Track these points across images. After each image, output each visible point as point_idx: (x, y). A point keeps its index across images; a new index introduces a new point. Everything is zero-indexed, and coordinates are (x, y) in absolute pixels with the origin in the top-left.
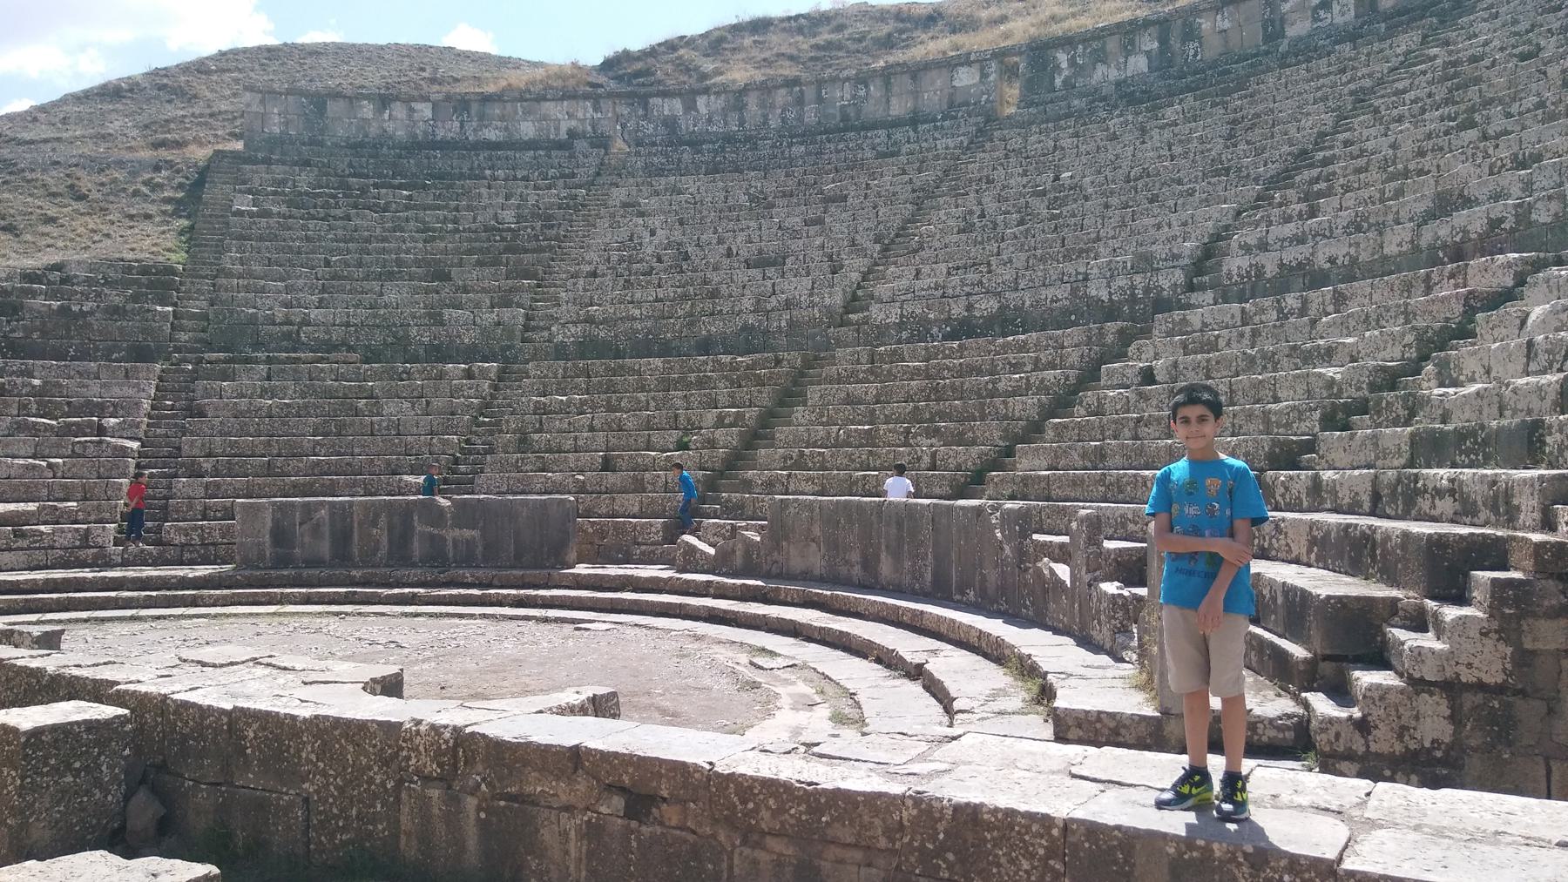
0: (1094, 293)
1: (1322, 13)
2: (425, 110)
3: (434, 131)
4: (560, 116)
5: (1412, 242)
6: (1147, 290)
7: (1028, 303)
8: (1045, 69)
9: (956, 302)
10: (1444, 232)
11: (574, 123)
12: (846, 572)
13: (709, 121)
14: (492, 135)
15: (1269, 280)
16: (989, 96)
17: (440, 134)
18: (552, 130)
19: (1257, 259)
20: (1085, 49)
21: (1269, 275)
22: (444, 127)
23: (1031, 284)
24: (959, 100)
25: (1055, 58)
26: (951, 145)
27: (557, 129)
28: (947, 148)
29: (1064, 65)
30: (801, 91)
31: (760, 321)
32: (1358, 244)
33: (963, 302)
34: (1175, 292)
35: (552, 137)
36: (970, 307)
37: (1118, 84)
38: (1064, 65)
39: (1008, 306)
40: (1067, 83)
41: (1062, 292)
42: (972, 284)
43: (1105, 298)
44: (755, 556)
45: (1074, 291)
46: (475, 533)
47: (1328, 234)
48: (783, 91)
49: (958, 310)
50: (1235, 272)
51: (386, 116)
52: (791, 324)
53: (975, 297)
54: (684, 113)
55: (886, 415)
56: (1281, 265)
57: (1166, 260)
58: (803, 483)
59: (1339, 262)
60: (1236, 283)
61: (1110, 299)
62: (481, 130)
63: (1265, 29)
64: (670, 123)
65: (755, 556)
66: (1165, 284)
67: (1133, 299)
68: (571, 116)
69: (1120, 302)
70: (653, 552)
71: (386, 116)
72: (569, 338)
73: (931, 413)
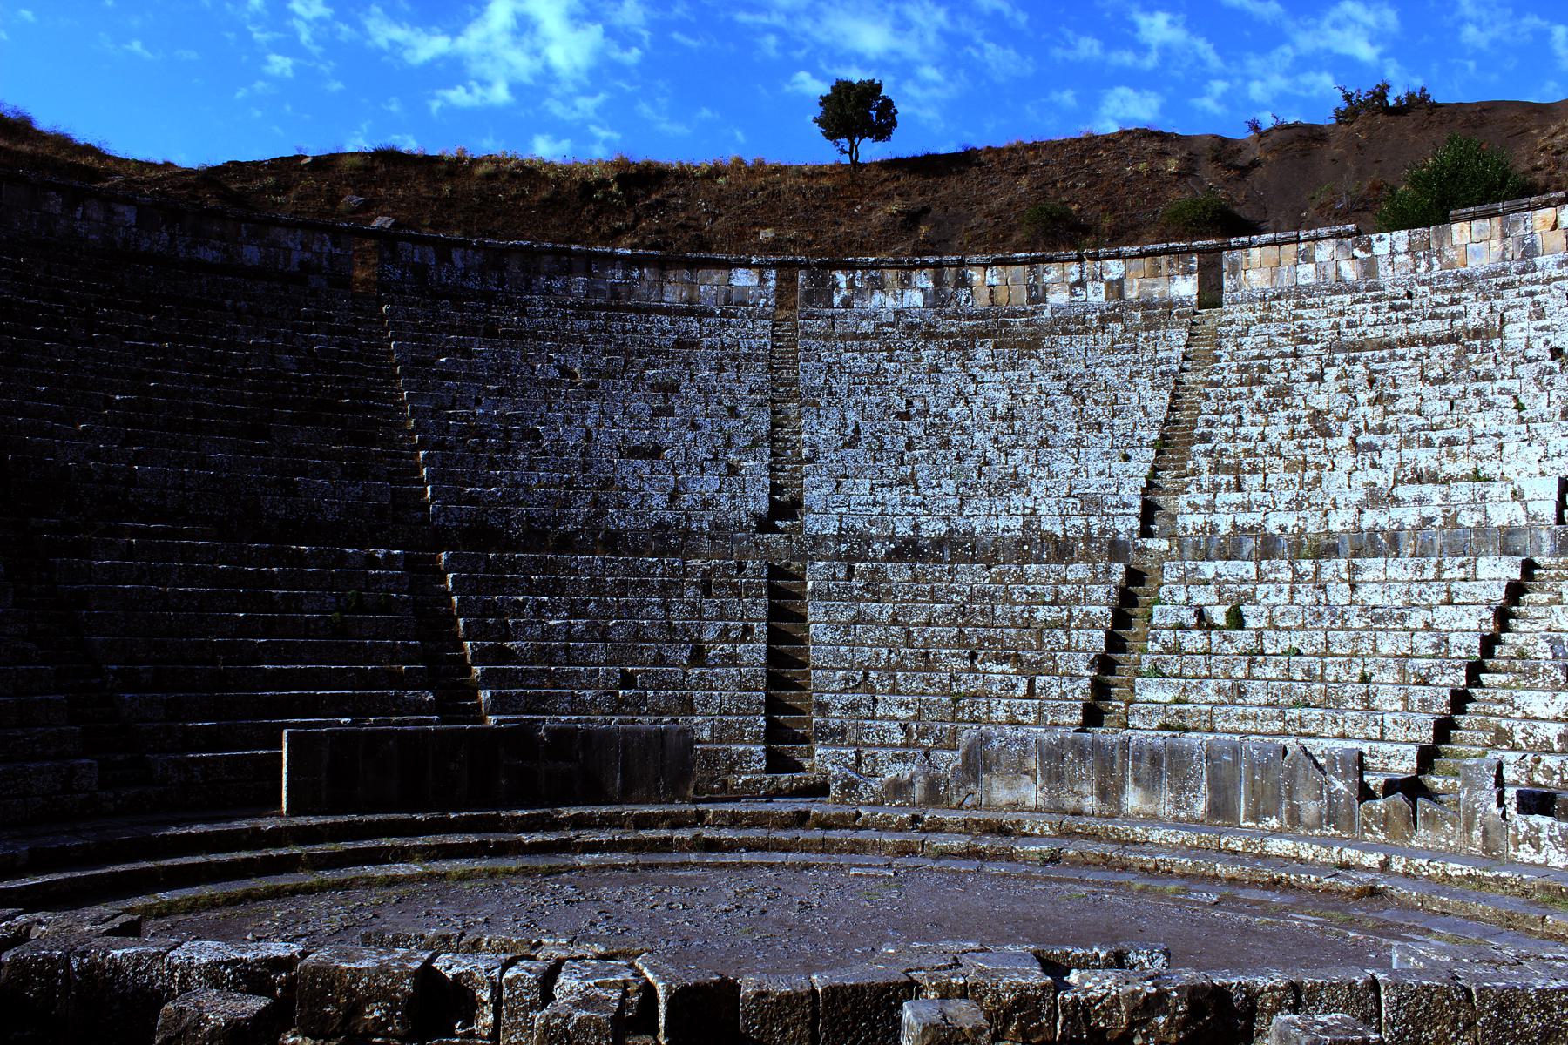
0: (1048, 528)
1: (1078, 289)
2: (129, 215)
3: (136, 240)
4: (291, 245)
5: (1354, 523)
6: (1103, 531)
7: (978, 530)
8: (824, 286)
9: (901, 521)
10: (1383, 520)
11: (307, 255)
12: (1074, 803)
13: (465, 276)
14: (207, 254)
15: (1223, 537)
16: (768, 300)
17: (145, 245)
18: (281, 259)
19: (1212, 518)
20: (863, 274)
21: (1222, 533)
22: (149, 238)
23: (975, 512)
24: (736, 298)
25: (834, 277)
26: (755, 345)
27: (288, 259)
28: (750, 348)
29: (843, 285)
30: (569, 261)
31: (678, 520)
32: (1305, 519)
33: (908, 521)
34: (1131, 536)
35: (280, 267)
36: (916, 527)
37: (897, 313)
38: (843, 285)
39: (957, 531)
40: (846, 303)
41: (1016, 523)
42: (914, 505)
43: (1060, 533)
44: (941, 788)
45: (1027, 524)
46: (285, 732)
47: (1271, 505)
48: (550, 258)
49: (903, 529)
50: (1190, 526)
51: (78, 214)
52: (715, 525)
53: (922, 519)
54: (437, 264)
55: (925, 639)
56: (1235, 526)
57: (1116, 507)
58: (895, 708)
59: (1289, 530)
60: (1191, 536)
61: (1065, 535)
62: (195, 248)
63: (1030, 293)
64: (421, 271)
65: (941, 788)
66: (1122, 529)
67: (1088, 538)
68: (305, 247)
69: (1074, 539)
70: (760, 782)
71: (78, 214)
72: (451, 521)
73: (979, 638)
